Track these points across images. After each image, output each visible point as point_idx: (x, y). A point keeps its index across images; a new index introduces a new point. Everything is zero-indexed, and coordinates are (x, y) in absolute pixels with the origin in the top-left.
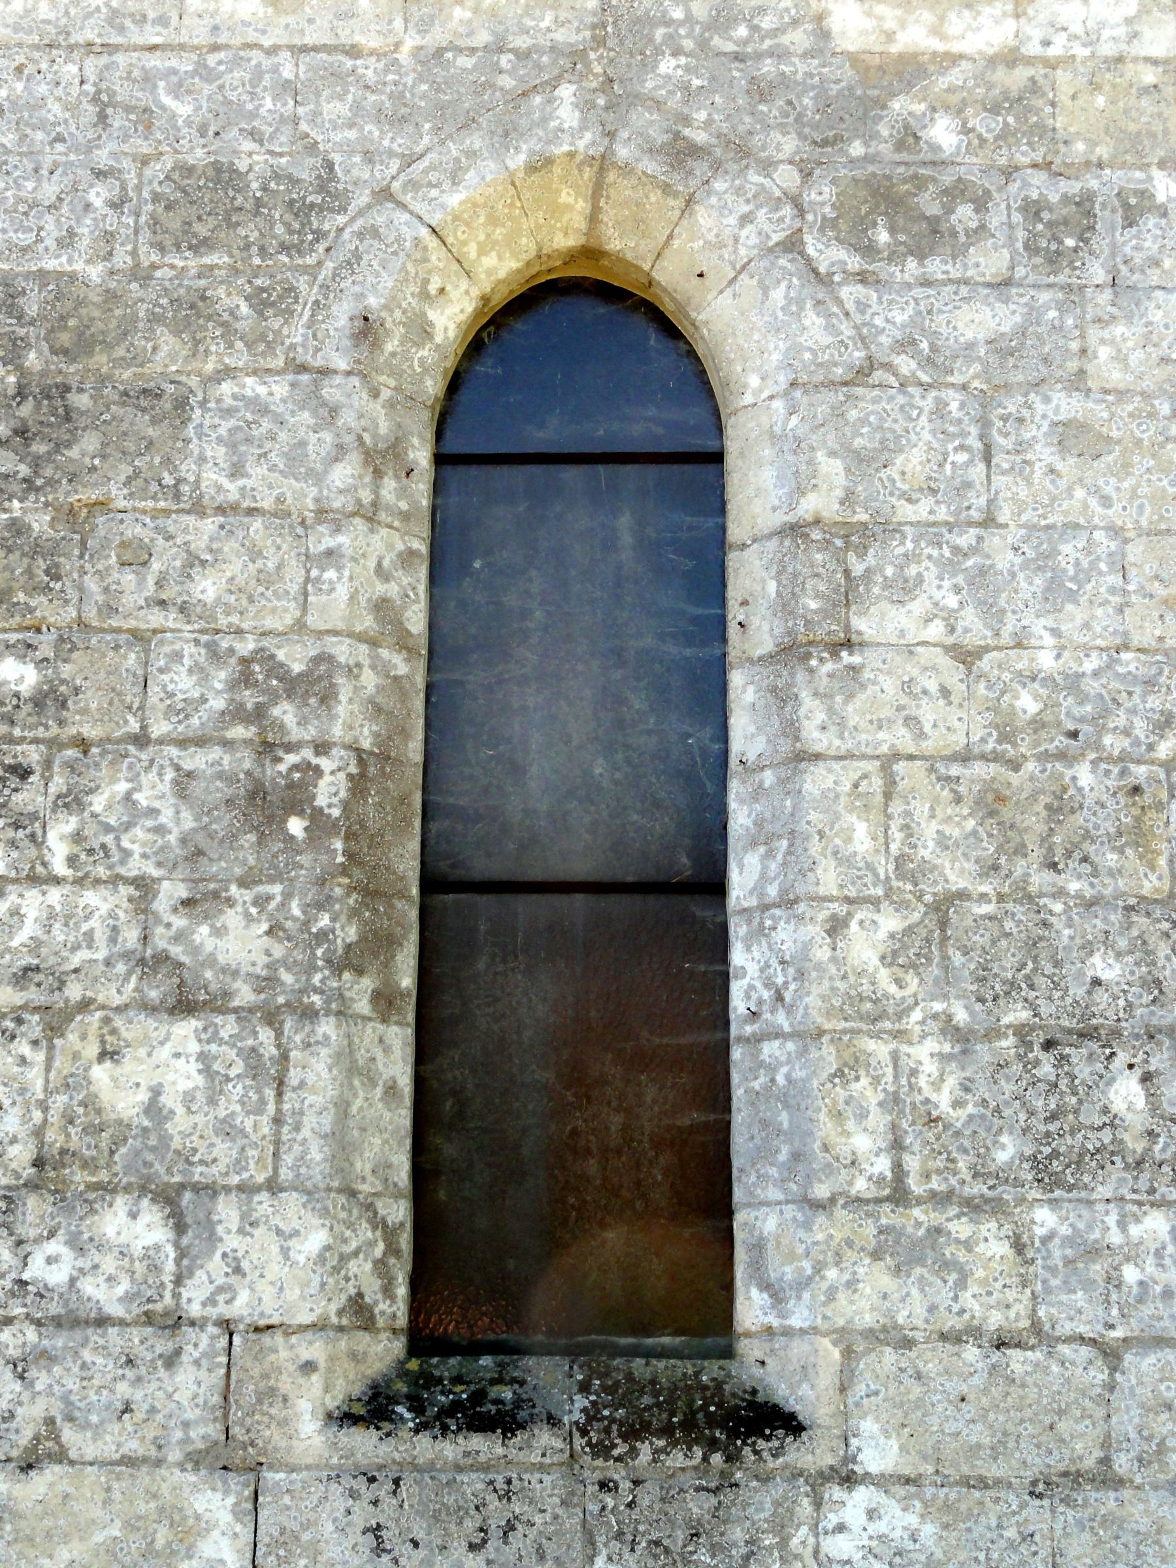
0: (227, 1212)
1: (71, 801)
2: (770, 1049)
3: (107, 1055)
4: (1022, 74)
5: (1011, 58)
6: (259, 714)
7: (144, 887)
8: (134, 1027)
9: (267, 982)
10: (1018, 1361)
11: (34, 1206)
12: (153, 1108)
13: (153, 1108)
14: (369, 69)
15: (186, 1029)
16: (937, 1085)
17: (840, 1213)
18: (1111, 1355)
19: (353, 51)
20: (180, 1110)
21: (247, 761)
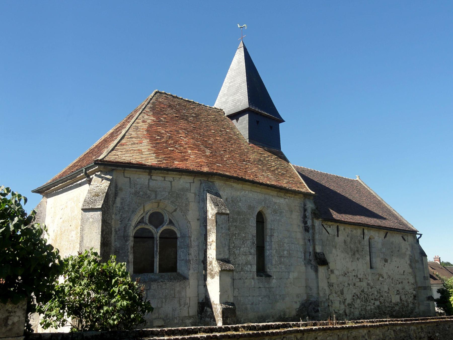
0: (253, 266)
1: (246, 243)
2: (270, 257)
3: (248, 257)
4: (279, 204)
5: (279, 203)
6: (253, 238)
7: (249, 247)
8: (249, 255)
9: (254, 253)
10: (279, 273)
11: (246, 265)
12: (250, 260)
13: (250, 260)
14: (256, 200)
15: (251, 256)
16: (320, 336)
17: (84, 233)
18: (282, 272)
19: (255, 198)
20: (438, 311)
21: (252, 241)
